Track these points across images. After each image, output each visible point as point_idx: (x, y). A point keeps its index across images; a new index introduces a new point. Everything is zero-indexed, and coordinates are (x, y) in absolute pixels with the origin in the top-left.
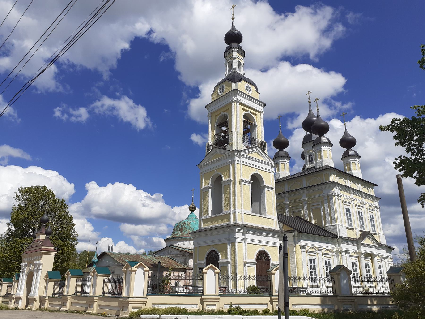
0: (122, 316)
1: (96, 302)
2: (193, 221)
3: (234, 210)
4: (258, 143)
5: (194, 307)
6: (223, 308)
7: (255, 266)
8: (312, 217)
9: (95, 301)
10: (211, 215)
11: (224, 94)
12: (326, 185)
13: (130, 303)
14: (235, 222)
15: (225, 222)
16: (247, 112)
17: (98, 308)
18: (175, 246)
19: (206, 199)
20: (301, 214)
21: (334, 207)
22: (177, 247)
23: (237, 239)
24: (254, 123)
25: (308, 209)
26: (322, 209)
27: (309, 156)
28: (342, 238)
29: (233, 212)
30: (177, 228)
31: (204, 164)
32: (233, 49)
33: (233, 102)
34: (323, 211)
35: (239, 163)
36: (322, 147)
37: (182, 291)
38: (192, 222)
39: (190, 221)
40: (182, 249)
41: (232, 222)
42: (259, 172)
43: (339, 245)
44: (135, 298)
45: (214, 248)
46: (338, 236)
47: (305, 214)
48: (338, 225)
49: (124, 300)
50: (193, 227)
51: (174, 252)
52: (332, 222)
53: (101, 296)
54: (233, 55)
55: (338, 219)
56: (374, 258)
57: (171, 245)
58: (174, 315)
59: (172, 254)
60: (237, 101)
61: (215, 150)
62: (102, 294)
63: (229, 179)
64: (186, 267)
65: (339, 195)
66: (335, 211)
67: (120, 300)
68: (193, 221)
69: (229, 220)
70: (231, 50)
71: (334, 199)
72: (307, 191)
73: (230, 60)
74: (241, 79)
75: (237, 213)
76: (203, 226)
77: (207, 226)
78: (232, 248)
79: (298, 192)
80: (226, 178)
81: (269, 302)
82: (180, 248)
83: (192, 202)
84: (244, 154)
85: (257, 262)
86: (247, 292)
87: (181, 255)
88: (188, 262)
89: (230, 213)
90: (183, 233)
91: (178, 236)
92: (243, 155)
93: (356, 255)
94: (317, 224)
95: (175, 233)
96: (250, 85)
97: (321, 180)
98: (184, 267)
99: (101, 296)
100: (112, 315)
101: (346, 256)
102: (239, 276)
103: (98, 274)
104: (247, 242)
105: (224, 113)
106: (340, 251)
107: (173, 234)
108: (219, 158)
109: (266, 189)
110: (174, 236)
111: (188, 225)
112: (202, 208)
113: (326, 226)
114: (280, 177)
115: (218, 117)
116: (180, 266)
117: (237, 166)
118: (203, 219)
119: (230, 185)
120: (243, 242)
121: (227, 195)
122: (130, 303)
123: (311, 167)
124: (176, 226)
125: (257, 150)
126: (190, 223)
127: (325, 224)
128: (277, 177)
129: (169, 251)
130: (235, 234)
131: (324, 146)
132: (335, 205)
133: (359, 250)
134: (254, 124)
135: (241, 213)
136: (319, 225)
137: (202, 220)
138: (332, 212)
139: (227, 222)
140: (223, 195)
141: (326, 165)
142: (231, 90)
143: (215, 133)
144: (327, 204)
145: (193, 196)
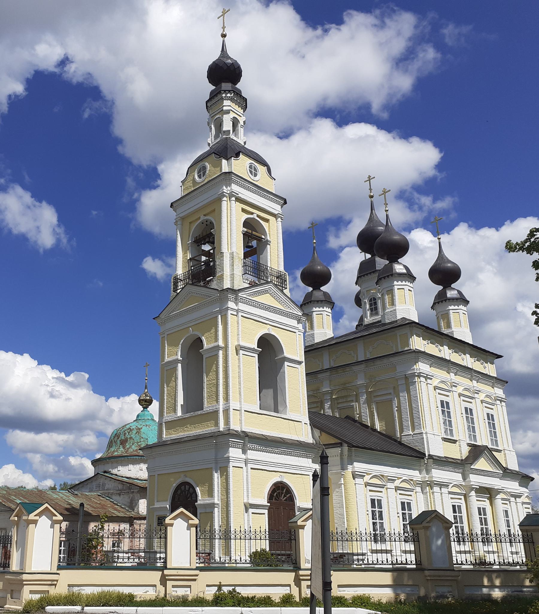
3: (225, 404)
4: (272, 276)
5: (148, 591)
6: (204, 593)
7: (266, 512)
10: (181, 415)
11: (206, 181)
12: (403, 357)
13: (24, 583)
16: (251, 216)
18: (112, 474)
19: (172, 384)
20: (355, 413)
22: (116, 475)
23: (230, 460)
25: (369, 402)
27: (370, 300)
28: (433, 459)
29: (223, 408)
30: (116, 439)
32: (224, 95)
33: (224, 196)
34: (396, 407)
35: (235, 313)
36: (395, 283)
37: (125, 560)
38: (144, 428)
39: (141, 425)
41: (222, 427)
42: (274, 332)
43: (428, 472)
44: (35, 573)
46: (425, 454)
47: (362, 411)
48: (426, 433)
49: (14, 577)
51: (110, 485)
56: (496, 497)
58: (110, 606)
59: (107, 490)
60: (231, 195)
61: (189, 290)
63: (216, 344)
64: (133, 514)
66: (421, 406)
67: (6, 577)
69: (217, 424)
71: (418, 384)
73: (217, 116)
74: (240, 152)
75: (231, 410)
76: (166, 435)
77: (173, 435)
79: (348, 370)
80: (210, 343)
82: (122, 477)
83: (145, 389)
84: (244, 296)
85: (269, 504)
87: (124, 490)
88: (137, 504)
89: (218, 411)
90: (128, 449)
91: (118, 454)
92: (242, 299)
94: (385, 430)
95: (112, 449)
98: (128, 514)
101: (441, 493)
102: (255, 532)
104: (250, 466)
105: (206, 218)
106: (429, 482)
107: (109, 449)
109: (286, 363)
110: (110, 455)
111: (136, 433)
113: (402, 434)
114: (314, 340)
116: (123, 512)
119: (217, 356)
120: (243, 465)
121: (212, 375)
122: (24, 583)
123: (375, 321)
125: (269, 288)
126: (141, 428)
127: (402, 431)
128: (308, 341)
130: (227, 451)
131: (399, 282)
132: (421, 394)
133: (466, 481)
137: (164, 424)
138: (415, 409)
142: (219, 174)
143: (189, 256)
145: (147, 378)
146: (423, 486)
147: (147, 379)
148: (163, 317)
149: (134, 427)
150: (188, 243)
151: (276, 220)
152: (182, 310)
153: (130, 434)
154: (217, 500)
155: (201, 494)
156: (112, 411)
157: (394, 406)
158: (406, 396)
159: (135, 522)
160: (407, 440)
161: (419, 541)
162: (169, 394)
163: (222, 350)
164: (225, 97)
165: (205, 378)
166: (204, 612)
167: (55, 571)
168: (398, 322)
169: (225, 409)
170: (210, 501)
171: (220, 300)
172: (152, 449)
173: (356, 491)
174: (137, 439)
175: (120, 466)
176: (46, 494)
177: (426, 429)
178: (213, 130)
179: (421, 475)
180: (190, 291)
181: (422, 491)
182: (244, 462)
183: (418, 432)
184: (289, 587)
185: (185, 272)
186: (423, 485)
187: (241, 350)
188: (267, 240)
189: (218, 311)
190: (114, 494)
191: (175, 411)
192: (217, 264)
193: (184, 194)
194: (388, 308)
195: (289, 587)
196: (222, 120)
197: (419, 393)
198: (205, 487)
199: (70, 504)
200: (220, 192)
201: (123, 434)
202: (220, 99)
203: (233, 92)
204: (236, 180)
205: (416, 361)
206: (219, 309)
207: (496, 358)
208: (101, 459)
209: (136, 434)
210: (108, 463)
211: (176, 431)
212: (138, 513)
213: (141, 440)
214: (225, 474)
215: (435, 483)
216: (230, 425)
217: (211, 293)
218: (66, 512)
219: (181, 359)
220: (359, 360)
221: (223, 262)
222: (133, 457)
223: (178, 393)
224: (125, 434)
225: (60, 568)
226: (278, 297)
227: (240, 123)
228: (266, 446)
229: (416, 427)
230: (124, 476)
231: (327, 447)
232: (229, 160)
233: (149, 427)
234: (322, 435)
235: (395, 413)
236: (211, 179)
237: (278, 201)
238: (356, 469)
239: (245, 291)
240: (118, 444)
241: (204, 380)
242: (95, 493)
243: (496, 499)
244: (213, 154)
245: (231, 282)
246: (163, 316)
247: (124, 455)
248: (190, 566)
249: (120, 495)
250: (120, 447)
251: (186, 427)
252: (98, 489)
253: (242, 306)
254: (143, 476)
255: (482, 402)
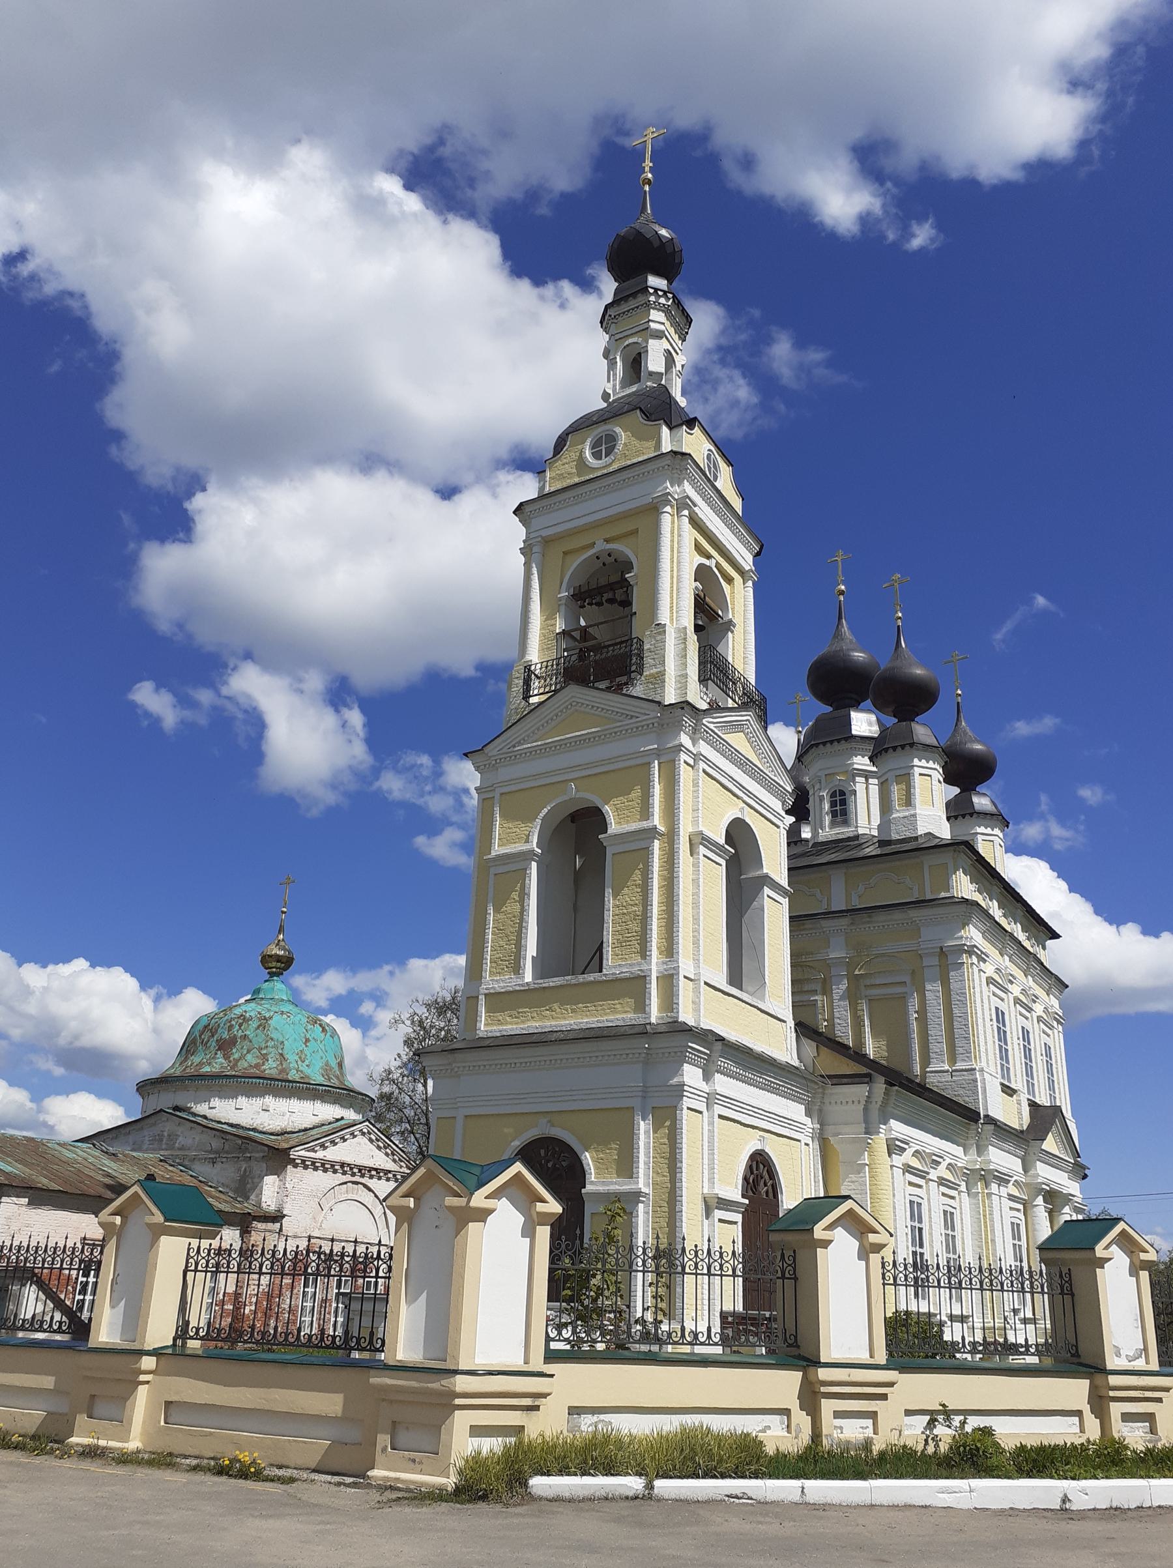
0: (397, 1479)
1: (148, 1382)
2: (282, 1013)
3: (664, 963)
5: (769, 1428)
6: (900, 1432)
7: (738, 1218)
8: (867, 1029)
9: (142, 1378)
10: (530, 980)
11: (615, 466)
12: (941, 910)
13: (458, 1401)
14: (671, 1017)
15: (614, 1011)
16: (707, 562)
17: (162, 1423)
18: (195, 1115)
19: (512, 907)
20: (820, 1016)
21: (966, 998)
22: (205, 1117)
23: (685, 1093)
24: (720, 613)
25: (852, 997)
26: (914, 1004)
27: (833, 795)
28: (995, 1124)
29: (658, 972)
30: (205, 1037)
31: (504, 750)
32: (652, 298)
33: (668, 502)
34: (915, 1012)
35: (691, 762)
36: (916, 762)
38: (276, 1018)
39: (269, 1010)
40: (225, 1126)
41: (655, 1014)
42: (751, 819)
43: (980, 1151)
45: (553, 1126)
46: (979, 1114)
47: (837, 1015)
48: (982, 1070)
49: (414, 1384)
50: (281, 1039)
51: (188, 1138)
52: (956, 1057)
53: (170, 1351)
54: (648, 322)
55: (979, 1046)
56: (1062, 1210)
57: (177, 1107)
58: (723, 1476)
59: (180, 1149)
60: (684, 504)
61: (573, 697)
62: (175, 1339)
63: (645, 824)
64: (248, 1207)
65: (983, 956)
66: (972, 1013)
67: (371, 1380)
68: (282, 1013)
69: (642, 1006)
70: (641, 299)
71: (968, 968)
72: (852, 923)
73: (631, 340)
75: (681, 978)
76: (485, 1025)
77: (510, 1027)
78: (655, 1132)
79: (810, 926)
80: (628, 822)
81: (1088, 1403)
82: (219, 1122)
83: (279, 933)
84: (712, 726)
85: (747, 1201)
86: (725, 1341)
87: (227, 1152)
88: (257, 1185)
89: (645, 976)
90: (237, 1061)
91: (214, 1070)
92: (707, 733)
93: (1018, 1195)
94: (887, 1060)
95: (196, 1059)
96: (719, 459)
97: (911, 889)
98: (239, 1208)
99: (167, 1347)
100: (287, 1467)
103: (166, 1220)
104: (718, 1110)
106: (983, 1173)
107: (186, 1059)
108: (593, 730)
109: (767, 891)
110: (191, 1071)
111: (258, 1027)
112: (484, 941)
113: (928, 1069)
115: (576, 562)
116: (226, 1202)
117: (685, 774)
118: (486, 995)
119: (647, 852)
120: (702, 1107)
121: (630, 894)
122: (458, 1401)
123: (841, 837)
124: (200, 1027)
125: (746, 720)
126: (271, 1018)
127: (926, 1061)
129: (166, 1134)
130: (678, 1070)
131: (923, 761)
132: (972, 990)
133: (1029, 1174)
134: (719, 616)
135: (691, 980)
136: (896, 1065)
137: (482, 997)
138: (959, 1019)
139: (626, 1012)
140: (608, 892)
141: (930, 833)
142: (652, 455)
143: (559, 626)
144: (935, 982)
145: (285, 910)
146: (971, 1181)
147: (285, 913)
148: (495, 752)
149: (252, 1014)
150: (559, 596)
151: (744, 584)
152: (550, 740)
153: (242, 1028)
154: (643, 1182)
155: (596, 1168)
156: (27, 991)
157: (911, 1010)
158: (939, 991)
159: (253, 1225)
160: (939, 1082)
161: (796, 1279)
162: (501, 930)
163: (659, 840)
164: (654, 302)
165: (609, 901)
166: (975, 1494)
167: (537, 1363)
168: (920, 841)
169: (666, 973)
170: (624, 1187)
171: (660, 727)
172: (456, 1055)
173: (893, 1183)
174: (258, 1039)
175: (217, 1099)
176: (45, 1147)
177: (981, 1062)
178: (618, 367)
179: (965, 1156)
180: (574, 699)
181: (967, 1189)
182: (705, 1100)
183: (964, 1067)
184: (1077, 1418)
185: (548, 661)
186: (970, 1177)
187: (701, 844)
188: (731, 621)
189: (654, 751)
190: (199, 1159)
191: (517, 969)
192: (645, 648)
193: (553, 489)
194: (898, 811)
195: (1077, 1418)
196: (645, 349)
197: (969, 987)
198: (608, 1151)
199: (109, 1175)
200: (659, 492)
201: (227, 1026)
202: (642, 305)
203: (673, 297)
204: (693, 475)
205: (966, 921)
206: (656, 746)
207: (1051, 939)
208: (170, 1079)
209: (256, 1029)
210: (186, 1089)
211: (516, 1018)
212: (258, 1205)
213: (269, 1044)
214: (667, 1123)
215: (995, 1175)
216: (678, 1012)
217: (638, 710)
218: (109, 1193)
219: (540, 851)
220: (833, 910)
221: (665, 645)
222: (251, 1080)
223: (527, 929)
224: (231, 1027)
225: (551, 1357)
226: (758, 745)
227: (675, 367)
228: (746, 1068)
229: (960, 1057)
230: (223, 1121)
231: (835, 1081)
232: (675, 430)
233: (289, 1017)
234: (821, 1054)
235: (913, 1024)
236: (629, 463)
237: (751, 544)
238: (894, 1135)
239: (715, 715)
240: (212, 1048)
241: (606, 903)
242: (151, 1155)
243: (1063, 1214)
244: (638, 411)
245: (678, 691)
246: (493, 749)
247: (228, 1073)
248: (872, 1356)
249: (214, 1163)
250: (218, 1056)
251: (547, 1010)
252: (155, 1146)
253: (704, 748)
254: (269, 1125)
255: (1039, 1019)
